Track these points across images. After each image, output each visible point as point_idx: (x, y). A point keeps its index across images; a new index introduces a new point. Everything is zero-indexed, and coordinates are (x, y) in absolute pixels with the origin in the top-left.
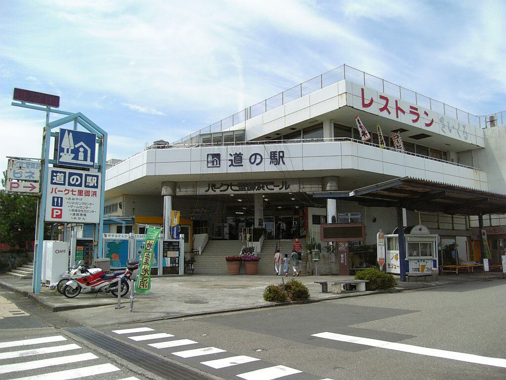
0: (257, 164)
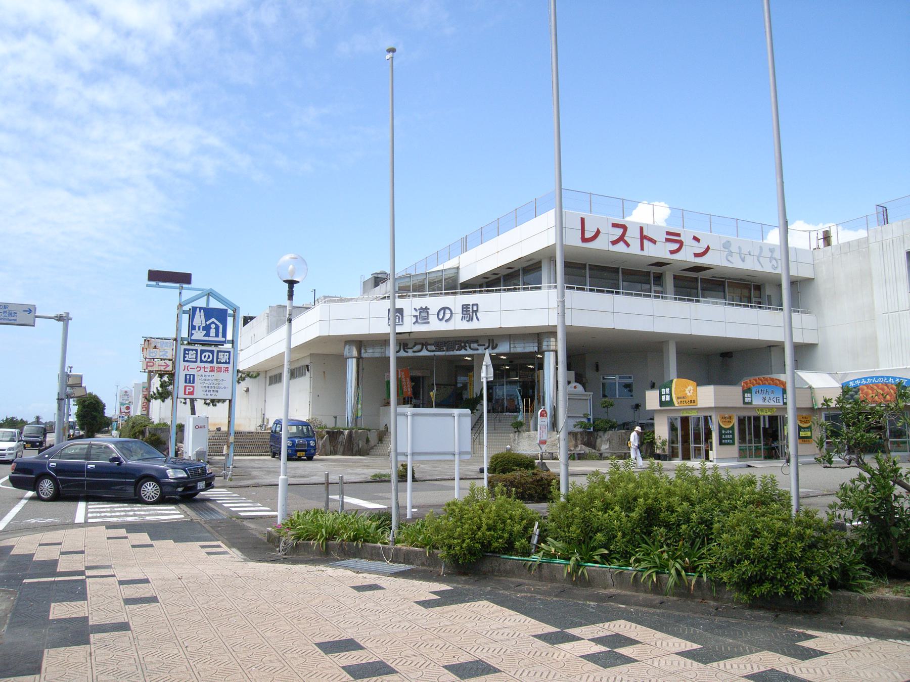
0: (447, 321)
